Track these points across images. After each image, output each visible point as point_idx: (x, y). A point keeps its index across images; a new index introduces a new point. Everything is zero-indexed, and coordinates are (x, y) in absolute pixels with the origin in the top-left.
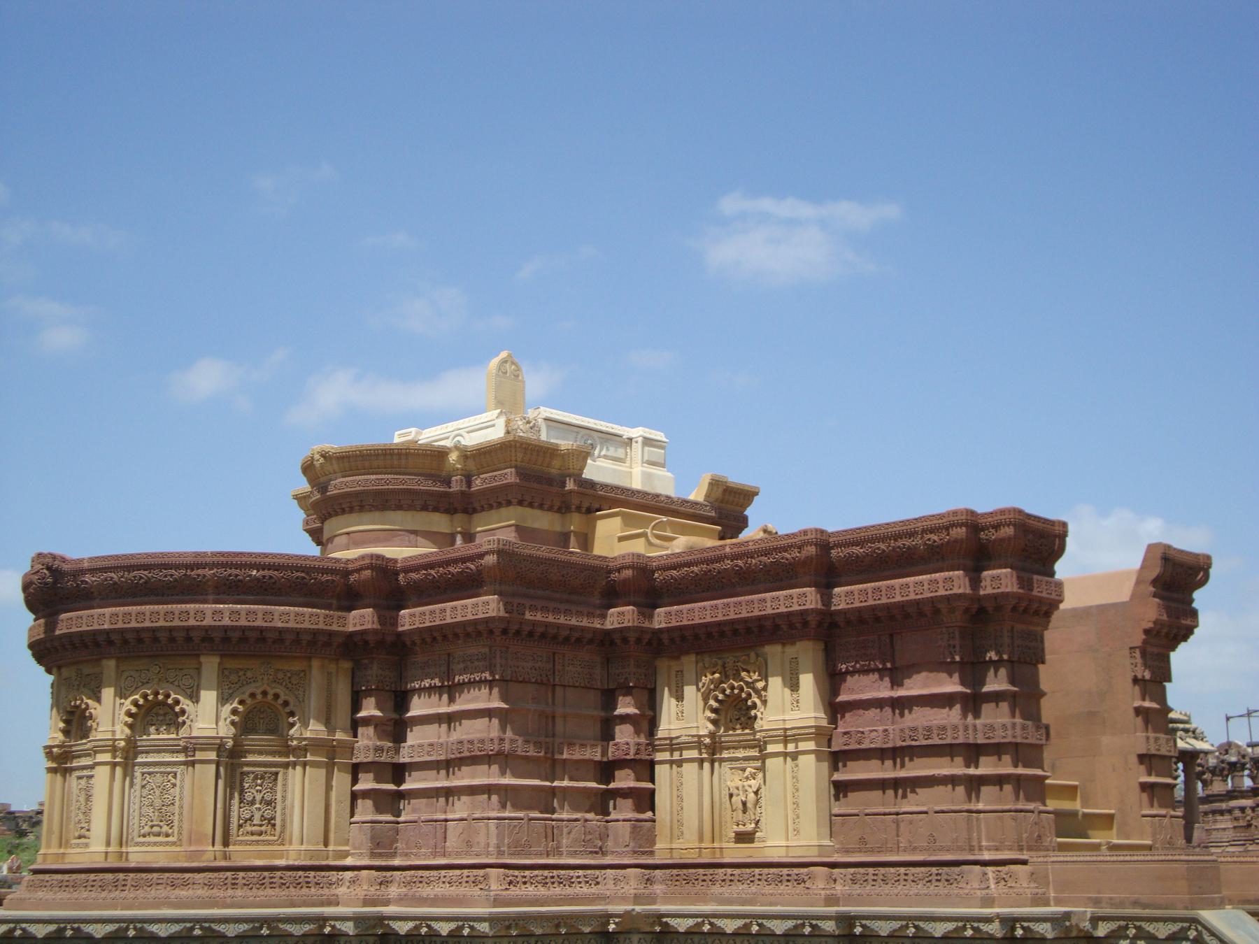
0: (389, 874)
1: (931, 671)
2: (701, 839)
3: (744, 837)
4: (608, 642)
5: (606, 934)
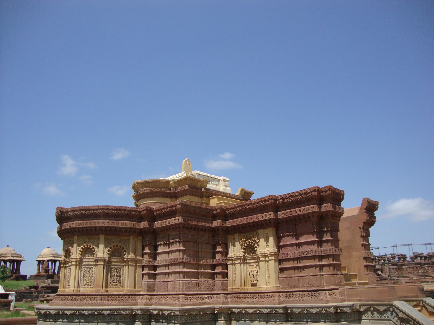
0: (152, 296)
1: (307, 235)
2: (241, 286)
3: (254, 285)
4: (213, 231)
5: (214, 314)
